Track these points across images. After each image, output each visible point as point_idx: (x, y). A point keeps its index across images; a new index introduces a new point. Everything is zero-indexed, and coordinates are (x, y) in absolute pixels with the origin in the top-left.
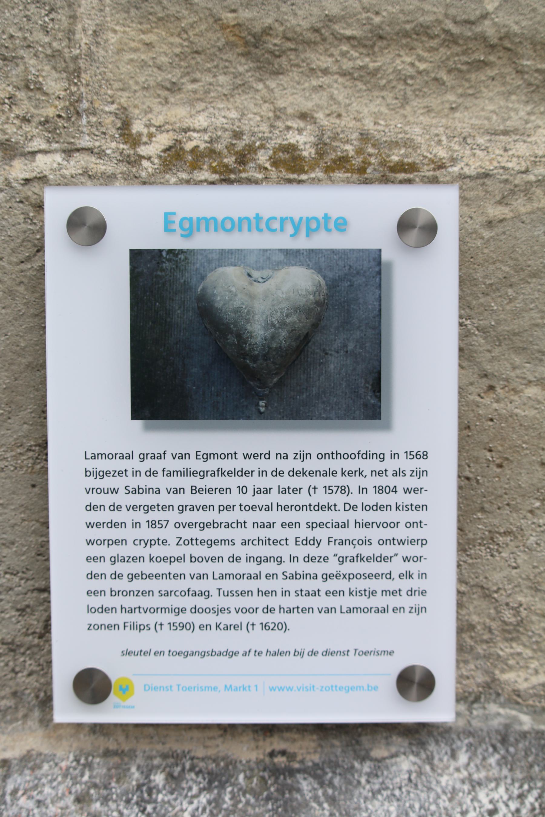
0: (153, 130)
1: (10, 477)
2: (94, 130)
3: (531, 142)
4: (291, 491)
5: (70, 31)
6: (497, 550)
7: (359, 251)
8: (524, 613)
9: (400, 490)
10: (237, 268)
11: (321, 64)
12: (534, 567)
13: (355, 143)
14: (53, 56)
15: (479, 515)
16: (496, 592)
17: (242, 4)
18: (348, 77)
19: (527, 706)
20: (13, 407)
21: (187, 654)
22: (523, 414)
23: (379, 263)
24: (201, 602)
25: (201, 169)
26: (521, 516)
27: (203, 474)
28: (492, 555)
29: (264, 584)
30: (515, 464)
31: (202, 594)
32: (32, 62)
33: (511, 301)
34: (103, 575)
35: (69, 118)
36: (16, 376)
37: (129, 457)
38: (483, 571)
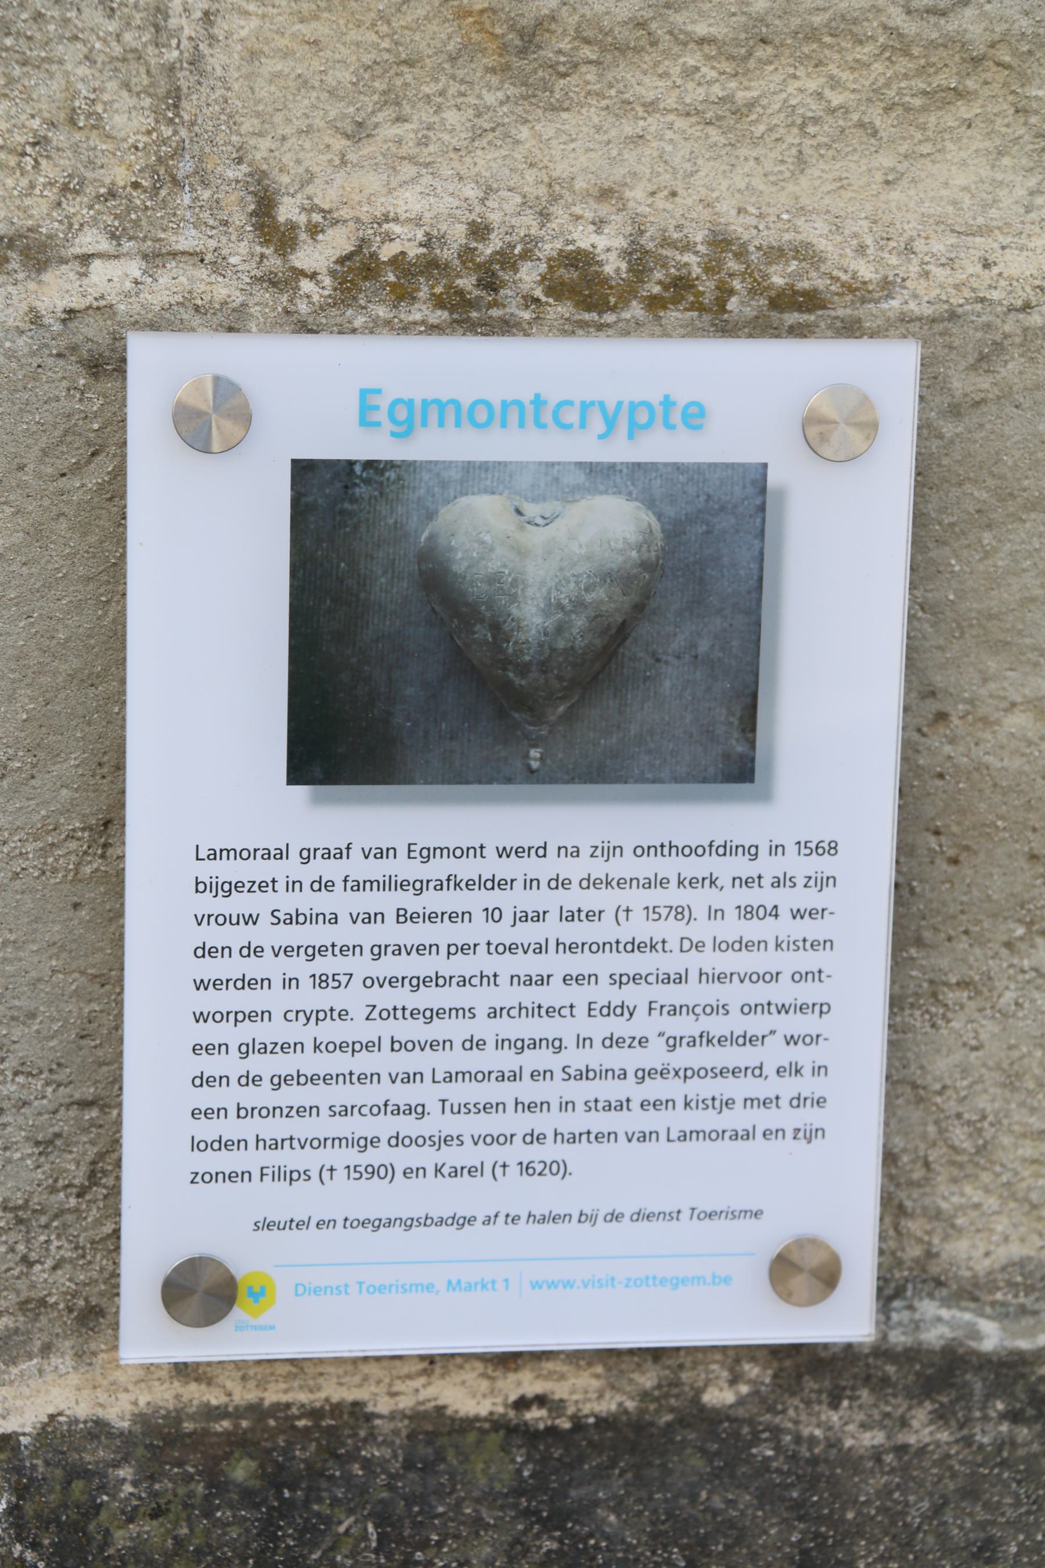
0: (317, 217)
1: (32, 890)
2: (205, 215)
3: (1033, 250)
5: (158, 9)
6: (944, 1016)
7: (727, 466)
8: (989, 1133)
9: (784, 913)
10: (496, 497)
11: (644, 92)
12: (1010, 1048)
13: (700, 248)
14: (124, 60)
15: (913, 952)
16: (940, 1093)
18: (693, 119)
19: (993, 1304)
20: (42, 755)
21: (378, 1225)
22: (999, 765)
23: (763, 490)
24: (408, 1126)
25: (414, 298)
26: (990, 953)
27: (420, 887)
28: (933, 1026)
29: (527, 1090)
30: (982, 855)
31: (410, 1110)
32: (83, 71)
33: (987, 555)
35: (156, 190)
36: (48, 696)
37: (281, 854)
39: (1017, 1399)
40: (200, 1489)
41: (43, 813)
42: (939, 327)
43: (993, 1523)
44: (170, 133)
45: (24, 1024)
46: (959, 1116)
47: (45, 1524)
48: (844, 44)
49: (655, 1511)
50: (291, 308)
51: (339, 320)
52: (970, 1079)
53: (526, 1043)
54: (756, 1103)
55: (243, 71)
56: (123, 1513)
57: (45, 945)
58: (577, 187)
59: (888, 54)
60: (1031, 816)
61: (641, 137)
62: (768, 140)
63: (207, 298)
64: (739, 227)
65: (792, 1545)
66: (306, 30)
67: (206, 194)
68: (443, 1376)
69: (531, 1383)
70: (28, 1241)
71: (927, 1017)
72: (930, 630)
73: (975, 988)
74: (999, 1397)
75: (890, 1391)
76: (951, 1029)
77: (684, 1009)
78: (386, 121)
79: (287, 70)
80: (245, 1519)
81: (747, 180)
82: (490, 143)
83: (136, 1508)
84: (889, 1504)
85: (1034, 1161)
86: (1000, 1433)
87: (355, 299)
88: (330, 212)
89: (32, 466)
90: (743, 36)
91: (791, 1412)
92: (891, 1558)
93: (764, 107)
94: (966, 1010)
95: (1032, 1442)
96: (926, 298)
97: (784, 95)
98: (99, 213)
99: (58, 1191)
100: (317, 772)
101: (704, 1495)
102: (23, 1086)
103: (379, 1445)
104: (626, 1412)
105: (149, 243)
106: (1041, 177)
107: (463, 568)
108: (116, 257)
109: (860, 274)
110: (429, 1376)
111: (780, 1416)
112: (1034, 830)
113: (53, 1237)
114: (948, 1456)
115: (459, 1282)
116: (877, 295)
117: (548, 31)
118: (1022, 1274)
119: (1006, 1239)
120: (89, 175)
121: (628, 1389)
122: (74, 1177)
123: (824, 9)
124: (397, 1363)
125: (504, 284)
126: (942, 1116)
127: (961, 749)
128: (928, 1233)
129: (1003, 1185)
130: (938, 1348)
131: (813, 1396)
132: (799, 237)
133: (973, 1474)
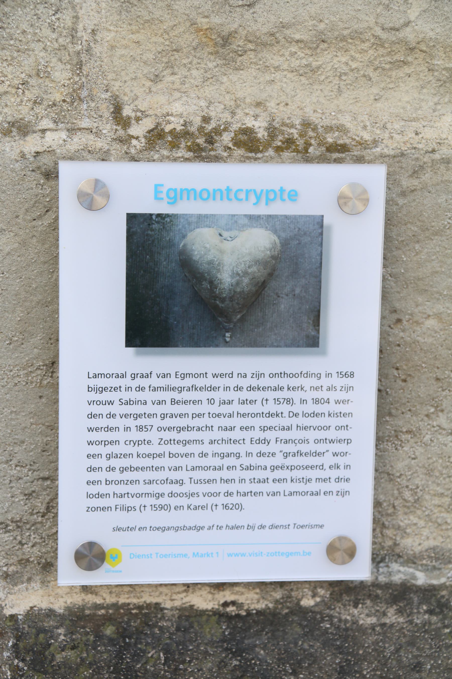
0: (139, 114)
2: (93, 113)
4: (248, 402)
6: (401, 445)
8: (420, 494)
9: (332, 402)
10: (211, 229)
11: (274, 62)
12: (429, 458)
14: (59, 50)
15: (388, 418)
16: (399, 477)
17: (213, 11)
18: (295, 74)
19: (422, 565)
20: (26, 335)
21: (164, 529)
22: (423, 341)
23: (322, 226)
24: (176, 488)
25: (179, 147)
26: (420, 419)
27: (181, 390)
28: (396, 449)
29: (226, 474)
30: (416, 379)
32: (42, 54)
33: (417, 254)
34: (100, 469)
35: (72, 103)
36: (29, 310)
38: (390, 461)
39: (432, 605)
40: (92, 638)
41: (27, 358)
42: (397, 159)
43: (421, 656)
44: (78, 79)
45: (19, 445)
46: (407, 487)
47: (28, 652)
48: (357, 43)
49: (280, 649)
50: (128, 151)
51: (148, 156)
52: (412, 471)
53: (225, 454)
54: (321, 480)
55: (108, 54)
56: (60, 647)
57: (28, 413)
58: (247, 102)
59: (375, 47)
60: (436, 362)
61: (273, 81)
62: (326, 82)
63: (93, 147)
64: (314, 118)
65: (336, 664)
66: (134, 37)
67: (93, 105)
68: (193, 593)
69: (230, 596)
70: (22, 535)
71: (394, 445)
72: (394, 285)
73: (414, 434)
74: (425, 604)
75: (379, 601)
76: (404, 450)
77: (291, 441)
78: (168, 75)
79: (126, 54)
80: (110, 651)
81: (317, 98)
82: (211, 83)
83: (65, 646)
84: (377, 647)
85: (439, 506)
86: (425, 619)
87: (154, 147)
88: (144, 112)
89: (21, 216)
90: (315, 39)
91: (337, 609)
92: (377, 670)
93: (324, 69)
94: (410, 442)
95: (438, 623)
96: (392, 147)
97: (332, 64)
98: (50, 112)
99: (34, 514)
100: (138, 342)
101: (300, 643)
102: (19, 471)
103: (166, 621)
104: (269, 608)
105: (70, 125)
106: (439, 97)
107: (198, 258)
108: (56, 130)
109: (364, 137)
110: (187, 592)
111: (333, 611)
112: (438, 368)
113: (32, 534)
114: (403, 628)
115: (198, 553)
116: (371, 146)
117: (234, 37)
118: (434, 553)
119: (428, 538)
120: (45, 97)
121: (270, 599)
122: (40, 509)
123: (348, 28)
124: (174, 587)
125: (216, 141)
126: (400, 487)
127: (407, 334)
128: (395, 535)
129: (426, 516)
130: (399, 583)
131: (347, 602)
132: (339, 122)
133: (413, 636)
